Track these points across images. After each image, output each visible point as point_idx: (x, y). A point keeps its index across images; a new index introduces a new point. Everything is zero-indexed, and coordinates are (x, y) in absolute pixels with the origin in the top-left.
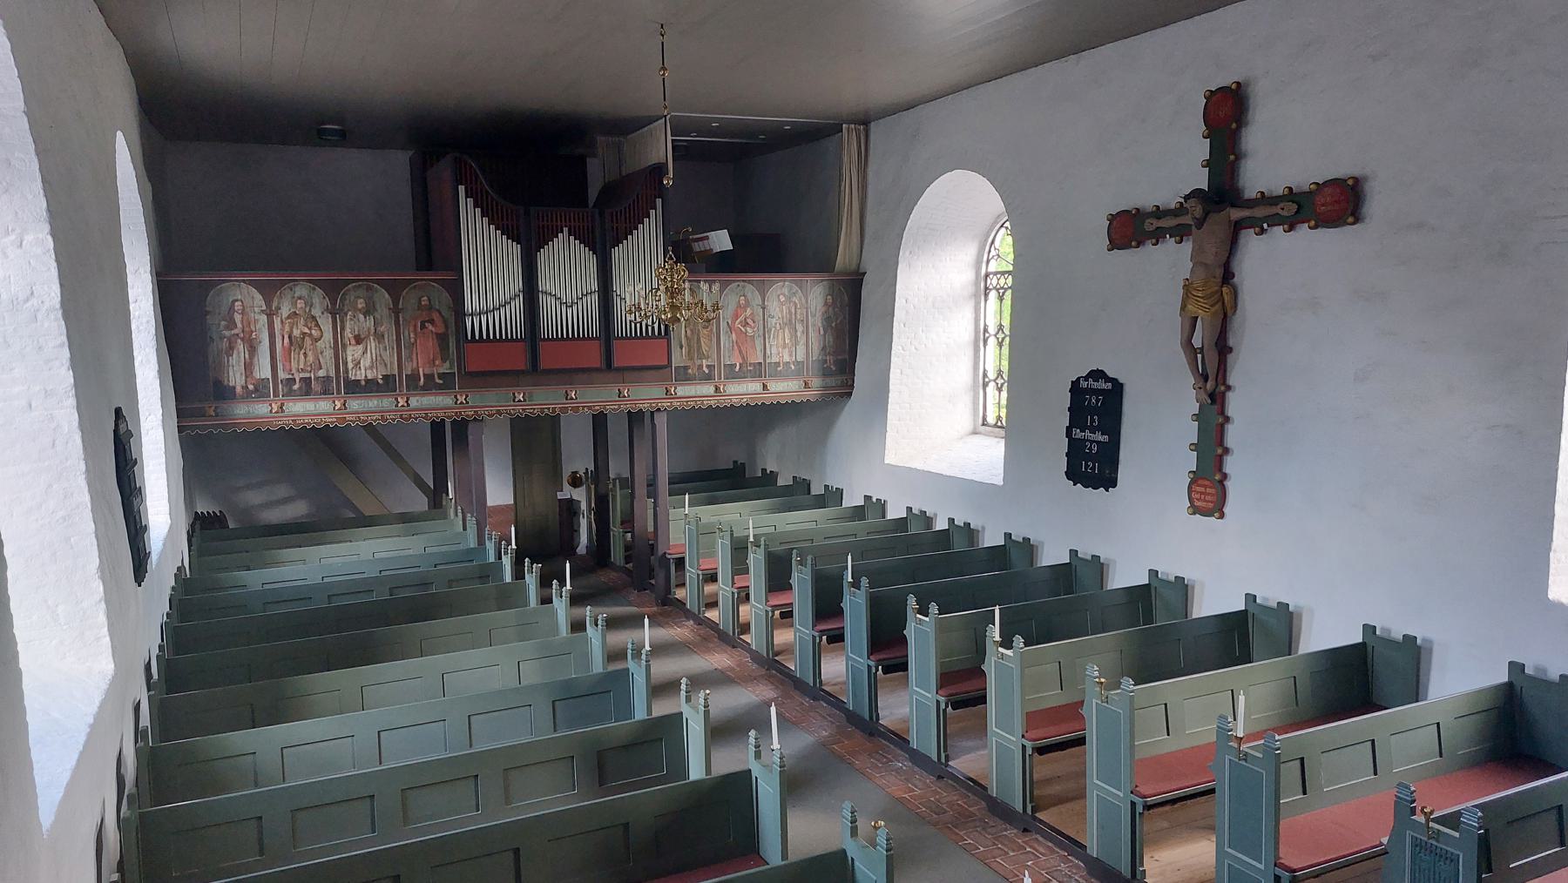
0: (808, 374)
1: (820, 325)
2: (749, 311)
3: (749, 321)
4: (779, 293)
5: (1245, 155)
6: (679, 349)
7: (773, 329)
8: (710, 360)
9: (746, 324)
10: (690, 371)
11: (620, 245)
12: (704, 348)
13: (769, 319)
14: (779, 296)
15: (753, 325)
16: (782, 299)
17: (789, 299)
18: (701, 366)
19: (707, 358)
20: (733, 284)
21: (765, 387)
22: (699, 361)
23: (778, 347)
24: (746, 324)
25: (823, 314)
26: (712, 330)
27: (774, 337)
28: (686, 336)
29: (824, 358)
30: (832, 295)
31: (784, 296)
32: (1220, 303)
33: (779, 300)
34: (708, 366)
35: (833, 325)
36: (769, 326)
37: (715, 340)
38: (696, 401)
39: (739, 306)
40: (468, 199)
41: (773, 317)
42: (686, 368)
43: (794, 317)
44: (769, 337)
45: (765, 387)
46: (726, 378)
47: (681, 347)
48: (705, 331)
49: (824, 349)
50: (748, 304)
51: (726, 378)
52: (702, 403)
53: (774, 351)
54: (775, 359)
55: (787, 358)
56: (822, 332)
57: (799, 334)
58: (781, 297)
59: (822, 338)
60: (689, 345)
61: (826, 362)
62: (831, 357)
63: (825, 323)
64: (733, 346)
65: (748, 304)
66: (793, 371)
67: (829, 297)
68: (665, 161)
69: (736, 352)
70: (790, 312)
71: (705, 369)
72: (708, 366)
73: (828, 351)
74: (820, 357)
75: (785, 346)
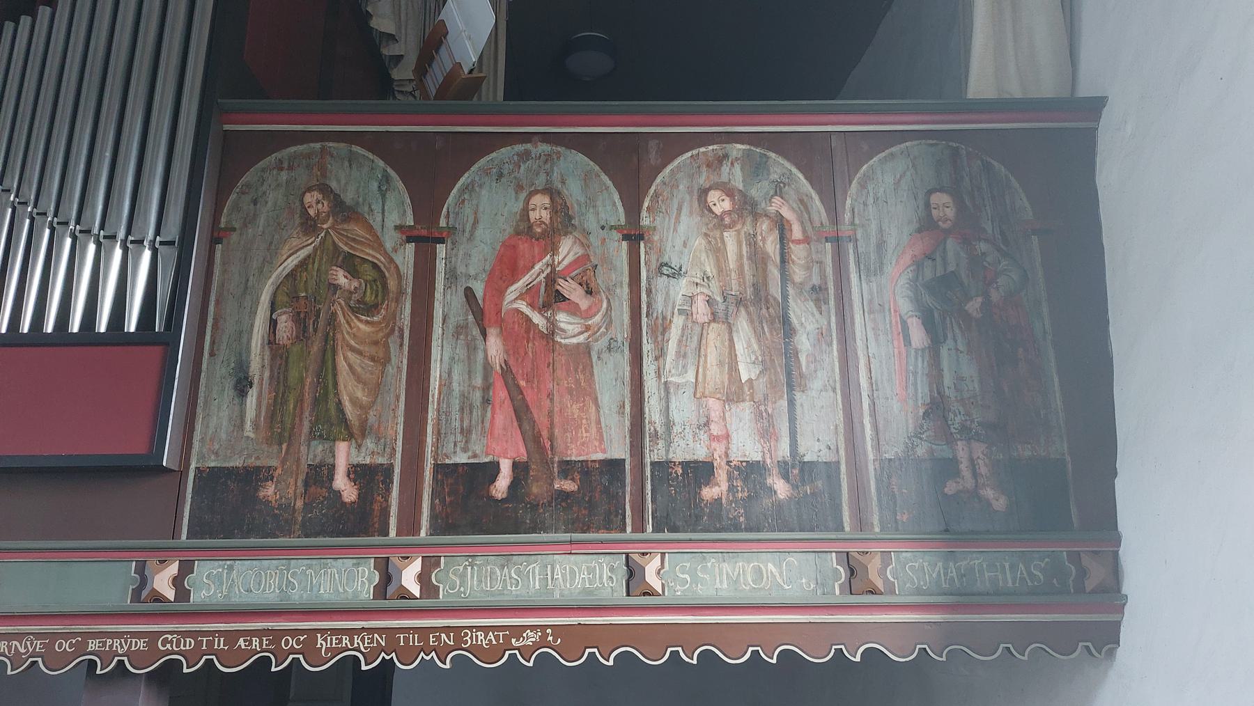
0: (861, 523)
1: (905, 306)
2: (567, 251)
3: (570, 289)
4: (703, 180)
5: (586, 296)
6: (229, 392)
7: (678, 321)
8: (369, 443)
9: (552, 298)
10: (269, 491)
11: (25, 21)
12: (350, 392)
13: (661, 282)
14: (704, 192)
15: (584, 303)
16: (720, 203)
17: (747, 207)
18: (321, 474)
19: (354, 434)
20: (505, 153)
21: (633, 573)
22: (319, 448)
23: (698, 394)
24: (552, 298)
25: (918, 265)
26: (393, 317)
27: (681, 355)
28: (271, 340)
29: (943, 451)
30: (955, 192)
31: (729, 192)
32: (577, 240)
33: (706, 208)
34: (359, 473)
35: (974, 306)
36: (659, 306)
37: (400, 360)
38: (277, 635)
39: (524, 228)
40: (827, 244)
41: (677, 274)
42: (252, 477)
43: (774, 273)
44: (660, 355)
45: (633, 573)
46: (442, 525)
47: (242, 385)
48: (362, 327)
49: (936, 408)
50: (563, 220)
51: (442, 525)
52: (309, 649)
53: (683, 409)
54: (688, 448)
55: (746, 446)
56: (918, 336)
57: (804, 343)
58: (713, 196)
59: (921, 366)
60: (280, 379)
61: (957, 473)
62: (979, 449)
63: (928, 299)
64: (486, 388)
65: (563, 220)
66: (779, 506)
67: (940, 199)
68: (727, 181)
69: (503, 416)
70: (758, 258)
71: (341, 482)
72: (359, 473)
73: (956, 421)
74: (921, 451)
75: (734, 393)
